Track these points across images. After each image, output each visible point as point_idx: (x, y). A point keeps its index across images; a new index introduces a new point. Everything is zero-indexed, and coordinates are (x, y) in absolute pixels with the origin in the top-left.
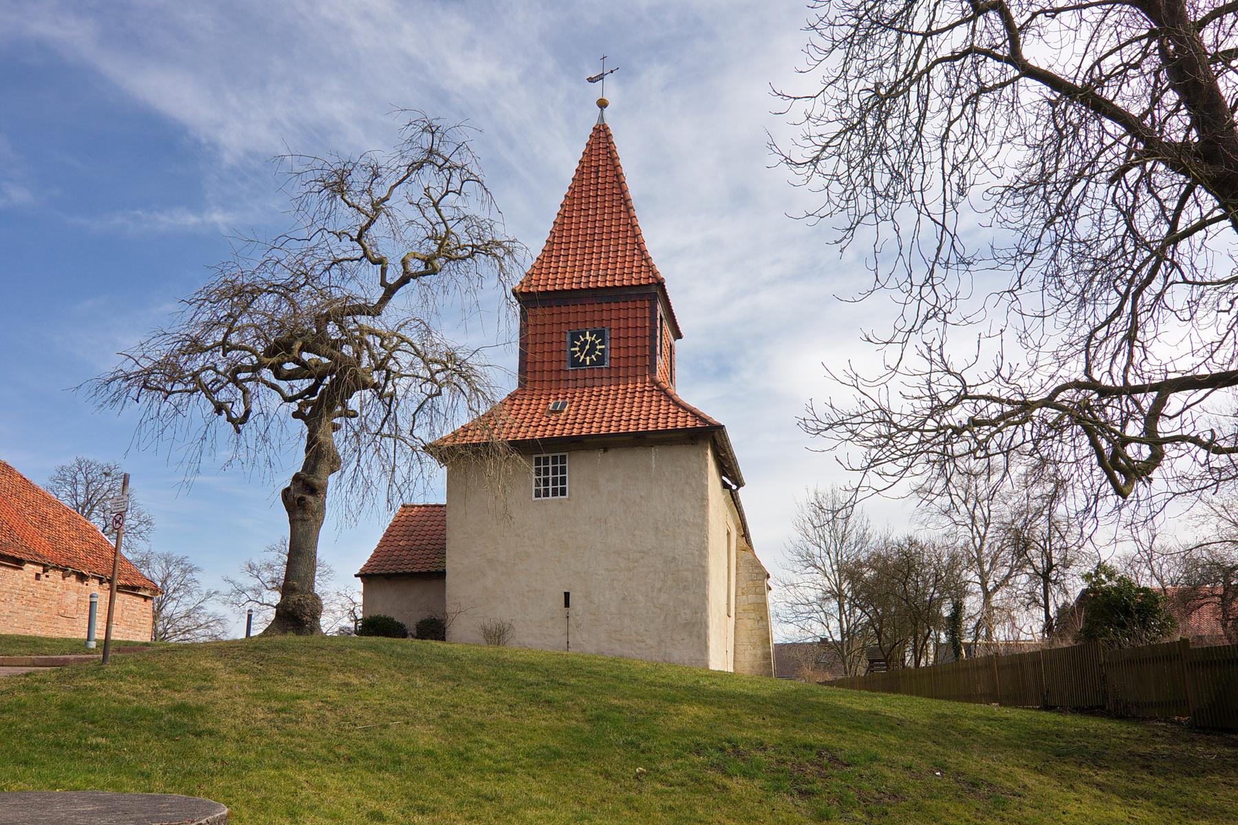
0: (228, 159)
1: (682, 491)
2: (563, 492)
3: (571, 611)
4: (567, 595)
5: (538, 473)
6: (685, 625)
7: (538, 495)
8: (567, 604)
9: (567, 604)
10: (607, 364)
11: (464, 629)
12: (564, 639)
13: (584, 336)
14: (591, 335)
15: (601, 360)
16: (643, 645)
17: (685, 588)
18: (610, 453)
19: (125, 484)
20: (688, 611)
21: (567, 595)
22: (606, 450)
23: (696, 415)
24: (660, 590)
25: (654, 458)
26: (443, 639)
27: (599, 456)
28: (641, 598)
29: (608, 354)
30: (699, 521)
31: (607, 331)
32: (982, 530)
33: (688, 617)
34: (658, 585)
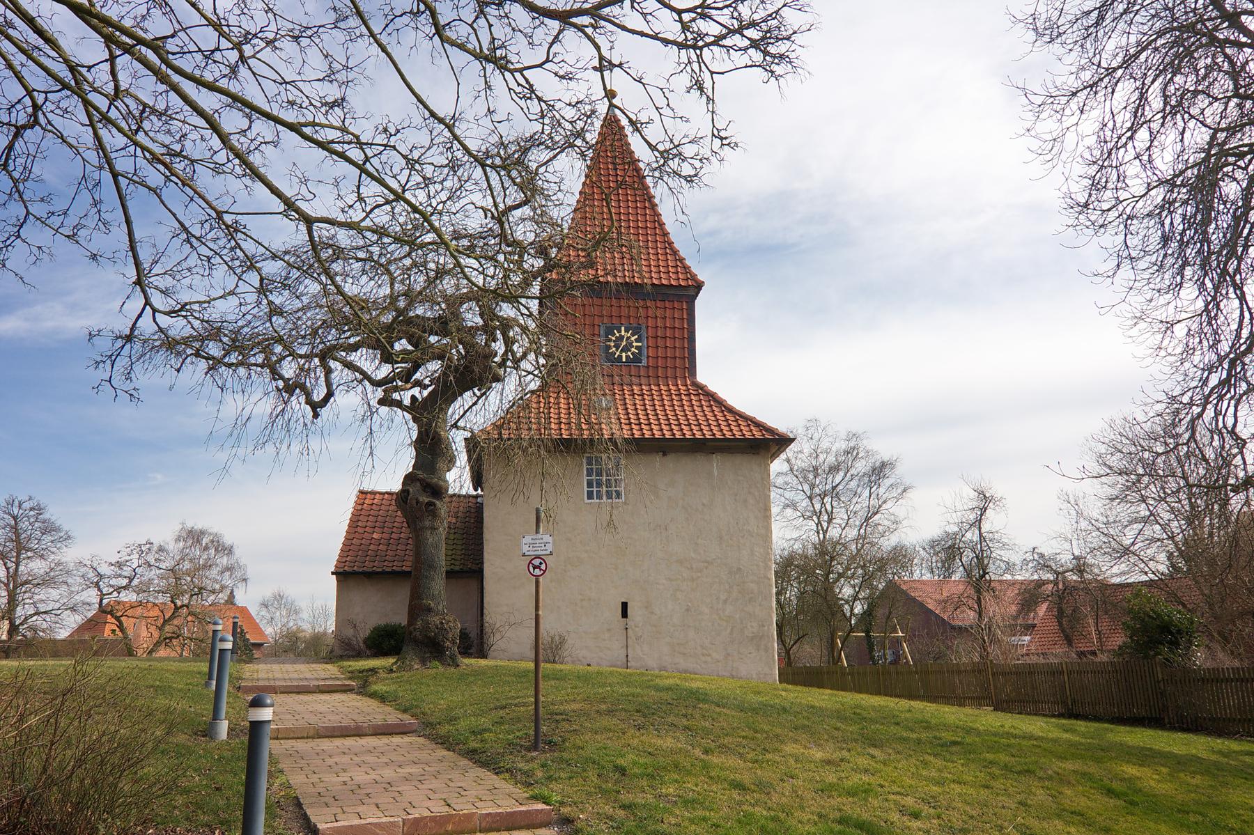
0: (451, 491)
1: (745, 501)
2: (619, 495)
3: (630, 621)
4: (625, 606)
5: (589, 473)
6: (752, 639)
7: (590, 496)
8: (625, 614)
9: (625, 614)
10: (644, 362)
11: (511, 644)
12: (623, 653)
13: (619, 331)
14: (627, 331)
15: (637, 359)
16: (709, 659)
17: (751, 600)
18: (670, 457)
19: (904, 491)
20: (755, 624)
21: (625, 606)
22: (664, 454)
23: (759, 425)
24: (725, 601)
25: (716, 465)
26: (483, 655)
27: (658, 459)
28: (707, 611)
29: (645, 351)
30: (763, 531)
31: (643, 327)
32: (825, 525)
33: (755, 630)
34: (723, 597)
